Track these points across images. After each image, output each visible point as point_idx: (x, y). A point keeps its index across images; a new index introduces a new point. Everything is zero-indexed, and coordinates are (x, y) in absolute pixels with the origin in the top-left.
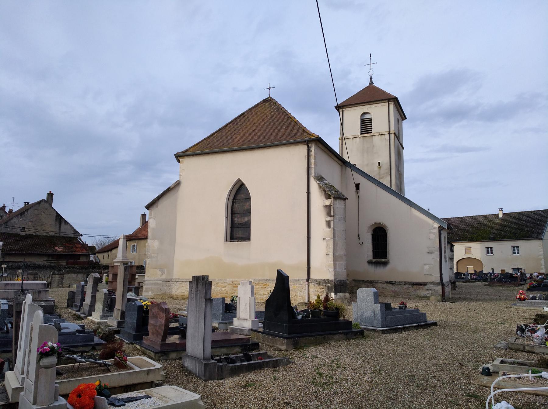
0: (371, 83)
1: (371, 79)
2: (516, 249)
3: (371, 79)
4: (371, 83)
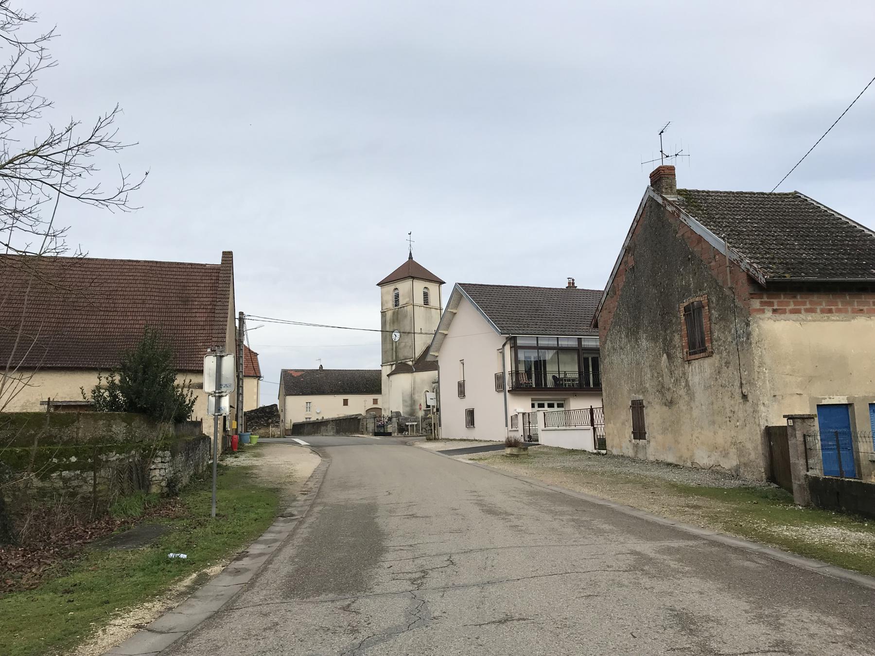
0: (411, 257)
1: (411, 254)
2: (346, 402)
3: (411, 254)
4: (411, 257)
